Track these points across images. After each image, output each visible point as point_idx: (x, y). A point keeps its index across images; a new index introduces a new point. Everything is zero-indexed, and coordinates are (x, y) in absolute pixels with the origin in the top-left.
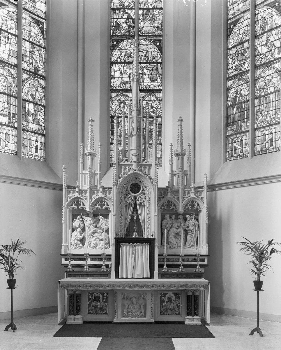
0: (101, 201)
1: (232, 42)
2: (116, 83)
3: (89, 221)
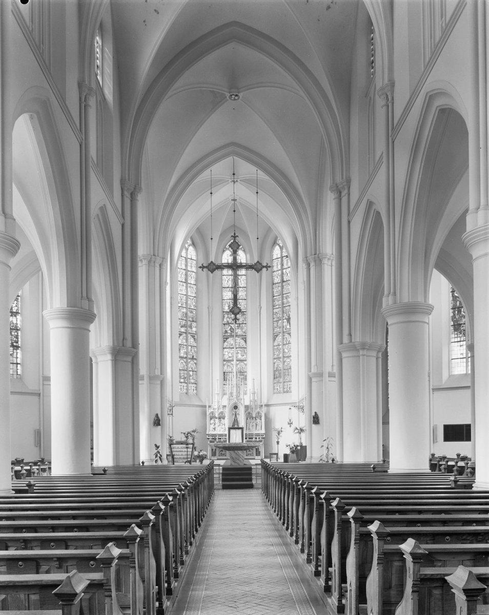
0: (222, 413)
1: (276, 344)
2: (226, 357)
3: (217, 420)
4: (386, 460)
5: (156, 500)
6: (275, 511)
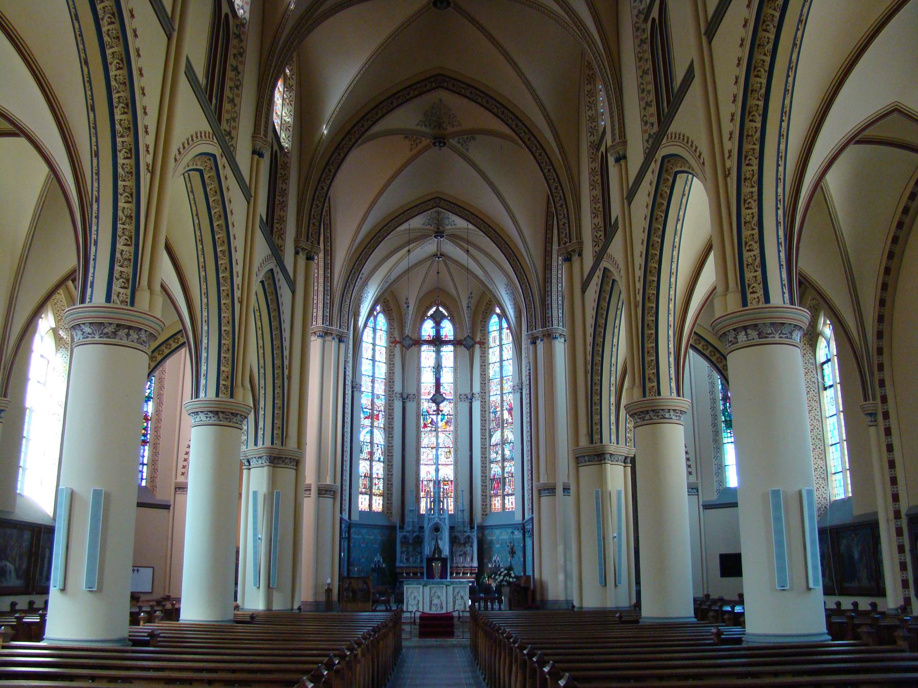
4: (638, 605)
5: (317, 663)
6: (484, 679)
